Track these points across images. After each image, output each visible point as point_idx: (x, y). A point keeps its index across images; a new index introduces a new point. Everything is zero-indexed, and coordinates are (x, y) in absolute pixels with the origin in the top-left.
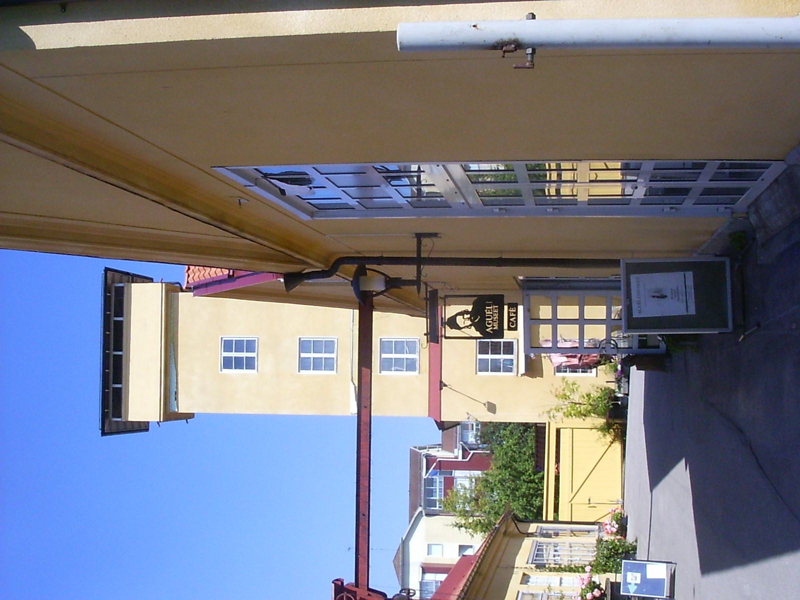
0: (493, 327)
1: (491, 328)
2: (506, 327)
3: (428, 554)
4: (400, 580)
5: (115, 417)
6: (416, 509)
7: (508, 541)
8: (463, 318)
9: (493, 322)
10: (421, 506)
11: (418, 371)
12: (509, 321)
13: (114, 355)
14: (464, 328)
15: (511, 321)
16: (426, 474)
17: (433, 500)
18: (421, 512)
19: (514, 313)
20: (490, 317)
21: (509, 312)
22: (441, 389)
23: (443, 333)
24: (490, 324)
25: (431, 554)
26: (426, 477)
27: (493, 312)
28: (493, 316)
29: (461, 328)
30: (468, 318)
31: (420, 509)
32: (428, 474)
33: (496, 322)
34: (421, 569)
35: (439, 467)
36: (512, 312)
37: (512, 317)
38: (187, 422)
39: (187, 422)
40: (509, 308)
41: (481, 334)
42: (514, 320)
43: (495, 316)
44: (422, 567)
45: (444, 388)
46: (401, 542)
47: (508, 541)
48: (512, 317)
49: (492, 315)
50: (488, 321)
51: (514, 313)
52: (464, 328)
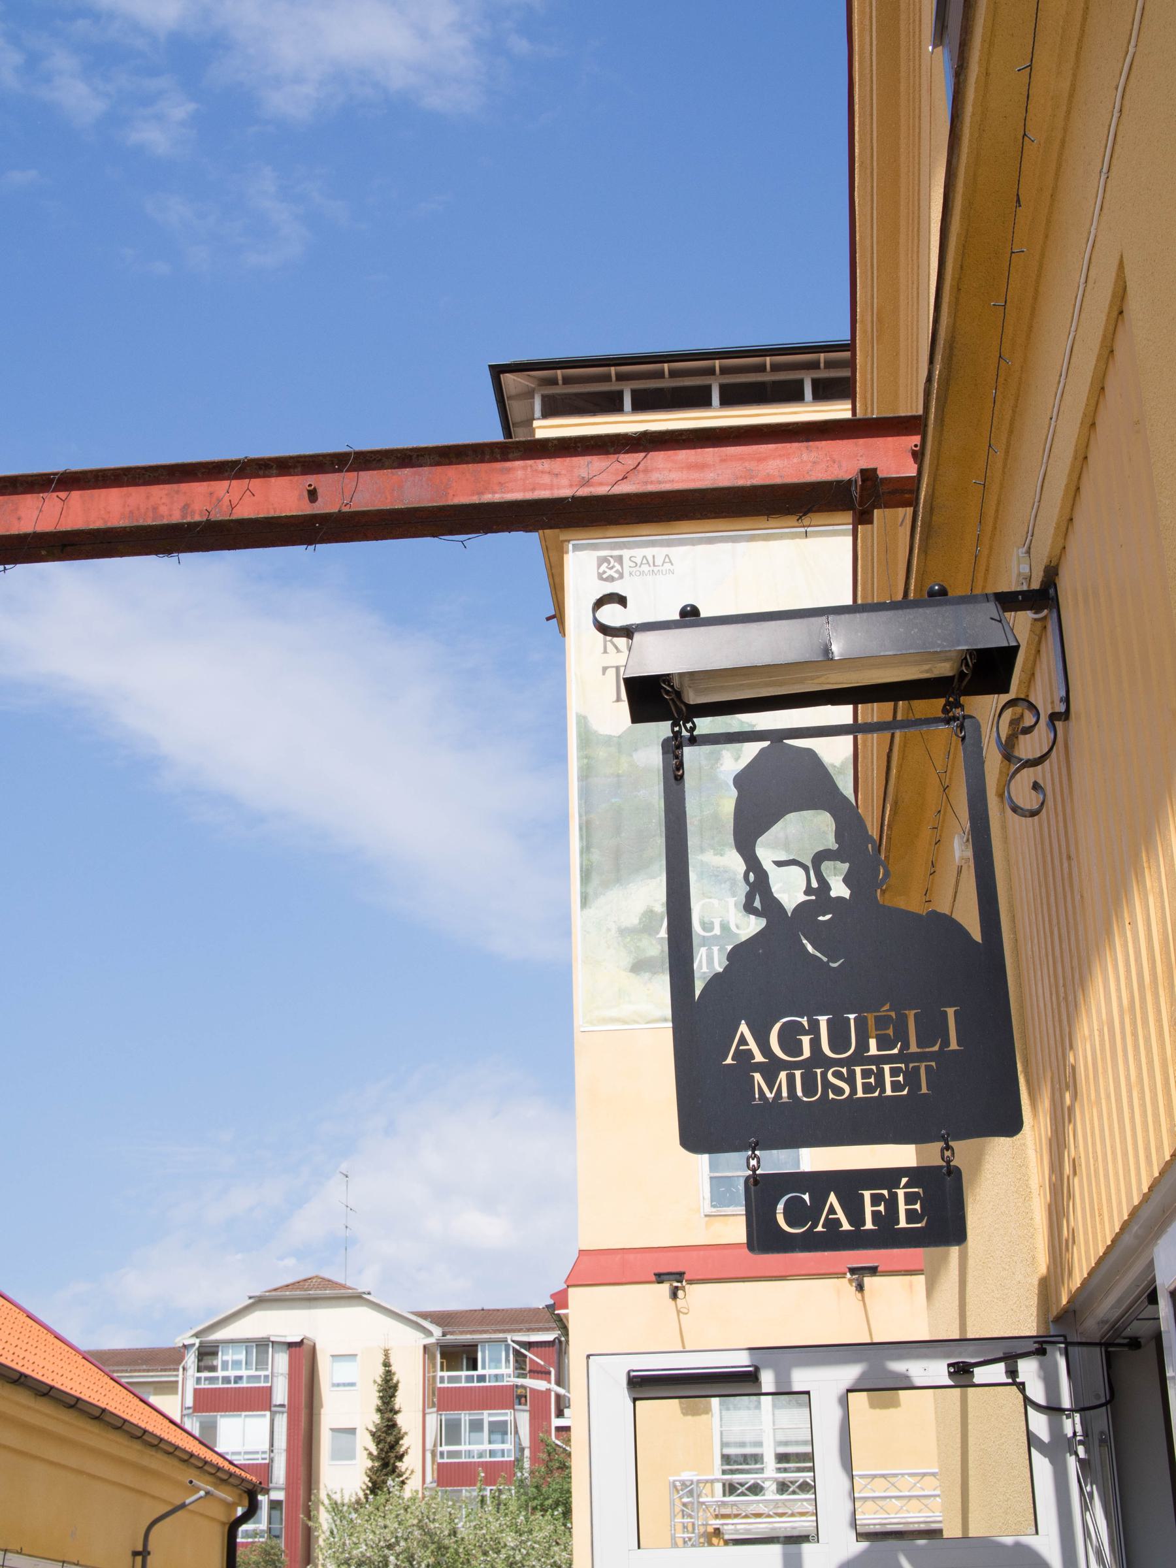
0: (771, 1069)
1: (759, 1058)
2: (775, 1161)
3: (332, 1356)
4: (267, 1294)
5: (543, 400)
6: (438, 1324)
7: (213, 1519)
8: (820, 857)
9: (807, 1067)
10: (444, 1335)
11: (713, 1211)
12: (821, 1182)
13: (708, 389)
14: (753, 863)
15: (820, 1200)
16: (513, 1341)
17: (462, 1364)
18: (429, 1333)
19: (886, 1220)
20: (839, 1040)
21: (886, 1177)
22: (660, 1278)
23: (705, 725)
24: (790, 1041)
25: (333, 1362)
26: (509, 1342)
27: (879, 1060)
28: (850, 1063)
29: (745, 843)
30: (825, 886)
31: (437, 1331)
32: (517, 1347)
33: (809, 1089)
34: (298, 1339)
35: (535, 1368)
36: (892, 1204)
37: (855, 1212)
38: (548, 619)
39: (548, 619)
40: (916, 1175)
41: (716, 981)
42: (833, 1224)
43: (851, 1081)
44: (302, 1341)
45: (665, 1288)
46: (360, 1291)
47: (213, 1519)
48: (855, 1212)
49: (860, 1057)
50: (814, 1029)
51: (886, 1220)
52: (753, 863)
